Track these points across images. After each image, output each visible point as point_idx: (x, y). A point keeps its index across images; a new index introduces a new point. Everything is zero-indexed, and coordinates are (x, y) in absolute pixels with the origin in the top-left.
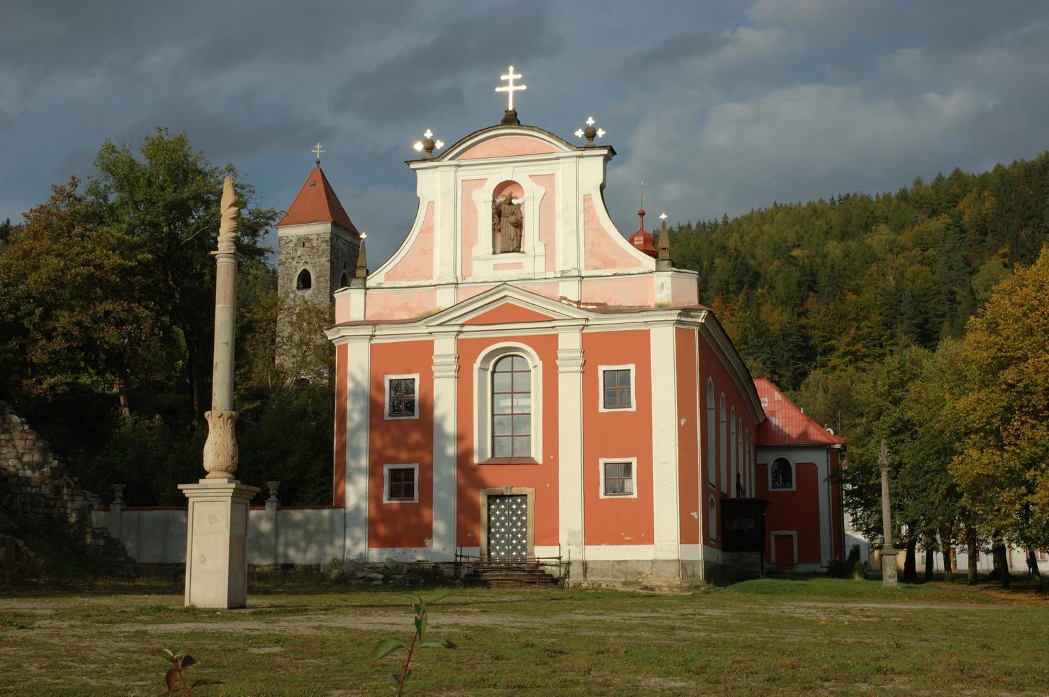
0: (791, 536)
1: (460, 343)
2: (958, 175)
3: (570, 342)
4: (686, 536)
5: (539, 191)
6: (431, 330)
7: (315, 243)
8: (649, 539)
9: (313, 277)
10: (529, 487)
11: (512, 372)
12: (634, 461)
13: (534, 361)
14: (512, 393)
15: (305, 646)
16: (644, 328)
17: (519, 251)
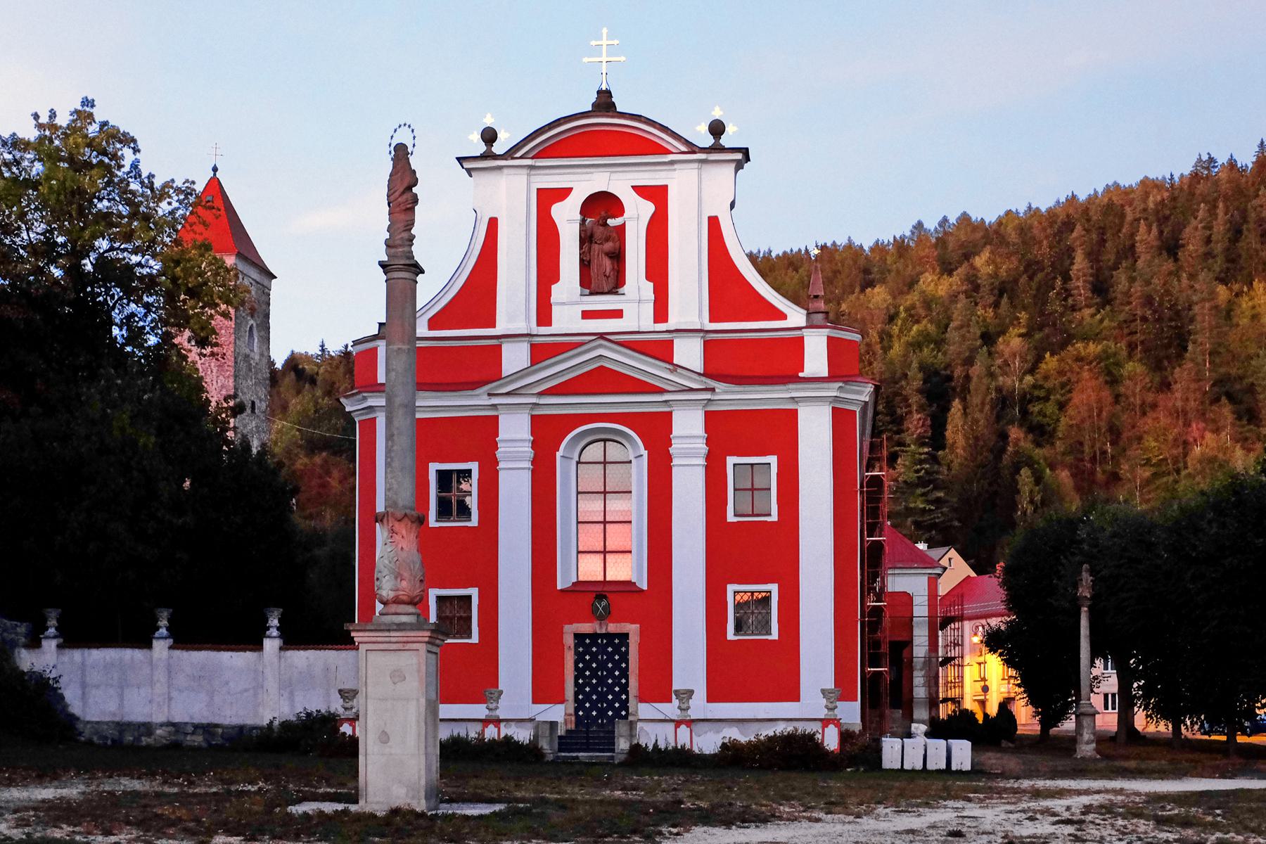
3: (688, 429)
4: (544, 691)
5: (648, 208)
8: (793, 694)
10: (632, 623)
11: (605, 522)
13: (636, 453)
14: (605, 493)
17: (616, 293)
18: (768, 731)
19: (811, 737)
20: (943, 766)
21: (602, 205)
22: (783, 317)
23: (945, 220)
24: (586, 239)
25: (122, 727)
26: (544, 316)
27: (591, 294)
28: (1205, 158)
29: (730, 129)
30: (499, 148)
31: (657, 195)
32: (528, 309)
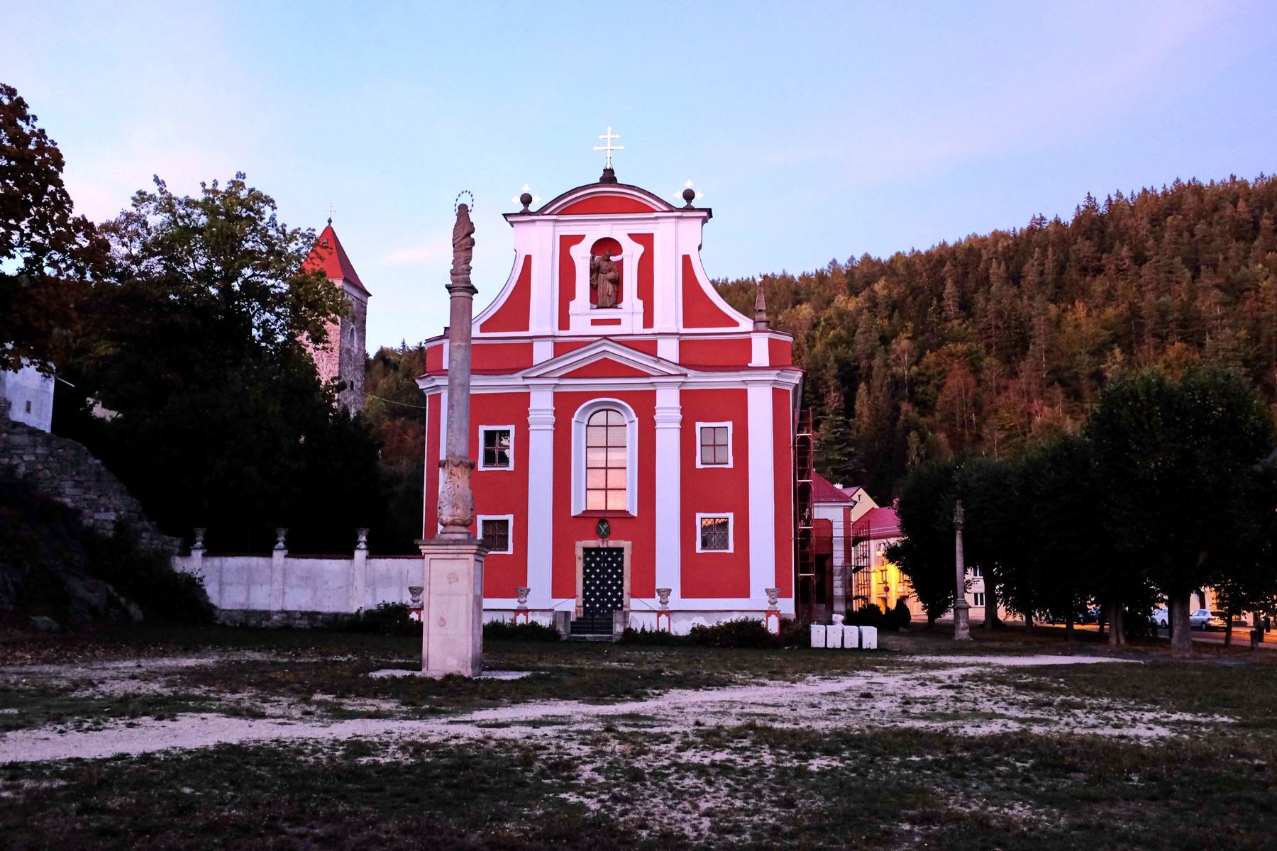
1: (557, 396)
2: (867, 258)
3: (668, 403)
4: (781, 590)
5: (640, 249)
6: (528, 382)
8: (746, 594)
13: (630, 419)
16: (743, 387)
18: (726, 619)
19: (758, 624)
21: (607, 247)
22: (737, 324)
23: (852, 258)
24: (595, 270)
26: (564, 322)
28: (1038, 217)
29: (698, 196)
30: (533, 207)
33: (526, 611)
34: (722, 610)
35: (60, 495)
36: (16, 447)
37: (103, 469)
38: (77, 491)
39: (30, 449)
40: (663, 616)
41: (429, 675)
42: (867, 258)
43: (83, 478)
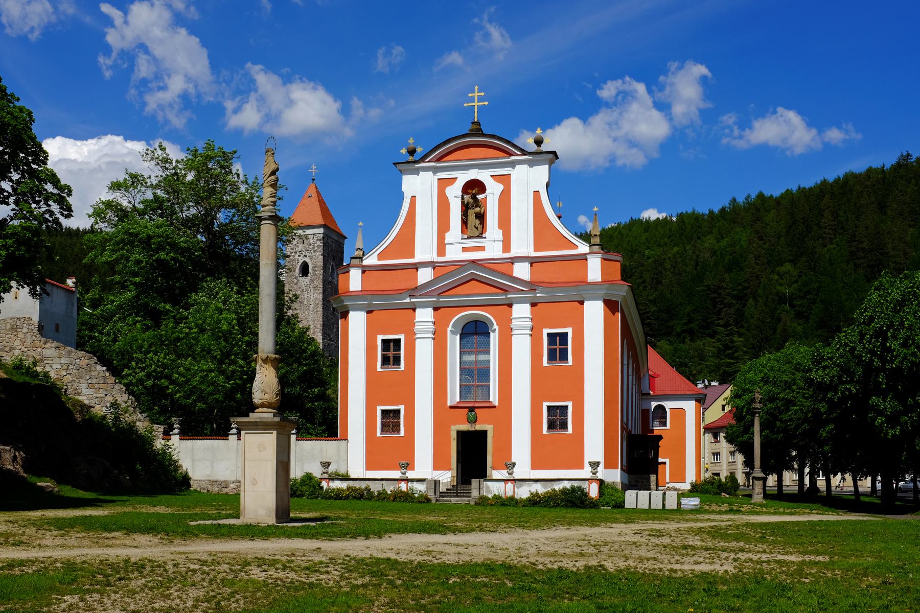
0: (399, 411)
2: (761, 196)
4: (438, 464)
5: (500, 187)
7: (311, 241)
9: (297, 270)
12: (570, 404)
15: (224, 526)
17: (481, 237)
18: (558, 487)
19: (580, 489)
20: (660, 507)
21: (474, 187)
22: (576, 247)
23: (749, 196)
24: (465, 208)
25: (213, 482)
26: (441, 251)
27: (468, 238)
28: (905, 154)
31: (505, 180)
32: (432, 246)
33: (407, 480)
34: (565, 477)
35: (79, 394)
36: (47, 358)
37: (107, 374)
38: (90, 391)
39: (57, 360)
40: (509, 484)
41: (249, 521)
42: (761, 196)
43: (94, 381)
